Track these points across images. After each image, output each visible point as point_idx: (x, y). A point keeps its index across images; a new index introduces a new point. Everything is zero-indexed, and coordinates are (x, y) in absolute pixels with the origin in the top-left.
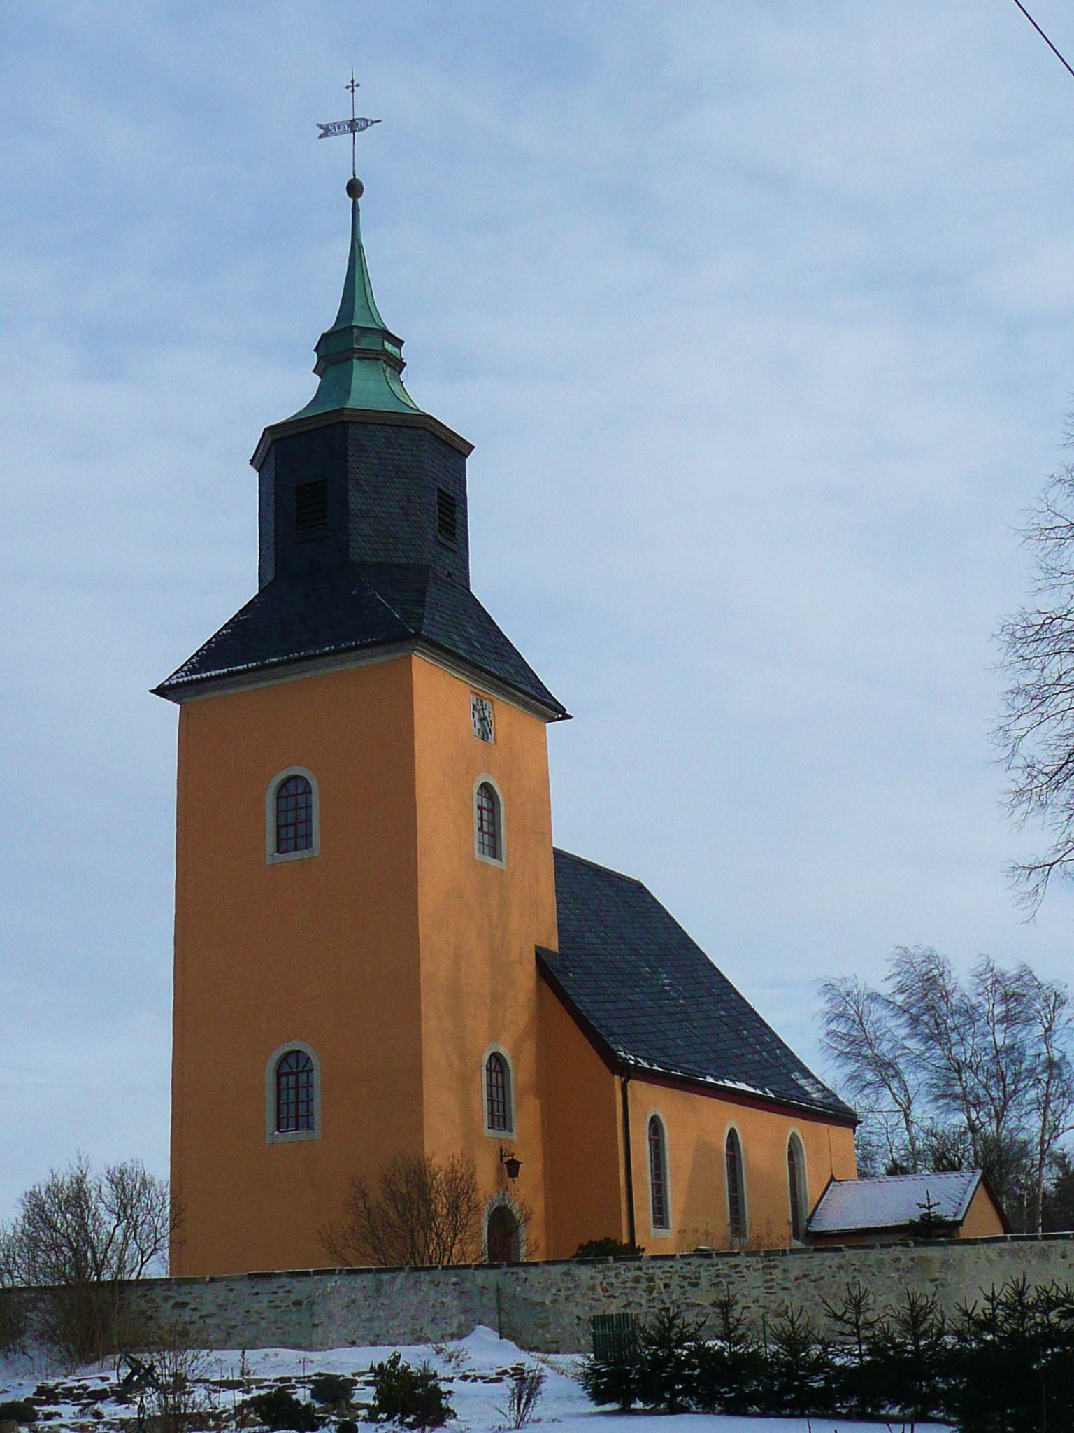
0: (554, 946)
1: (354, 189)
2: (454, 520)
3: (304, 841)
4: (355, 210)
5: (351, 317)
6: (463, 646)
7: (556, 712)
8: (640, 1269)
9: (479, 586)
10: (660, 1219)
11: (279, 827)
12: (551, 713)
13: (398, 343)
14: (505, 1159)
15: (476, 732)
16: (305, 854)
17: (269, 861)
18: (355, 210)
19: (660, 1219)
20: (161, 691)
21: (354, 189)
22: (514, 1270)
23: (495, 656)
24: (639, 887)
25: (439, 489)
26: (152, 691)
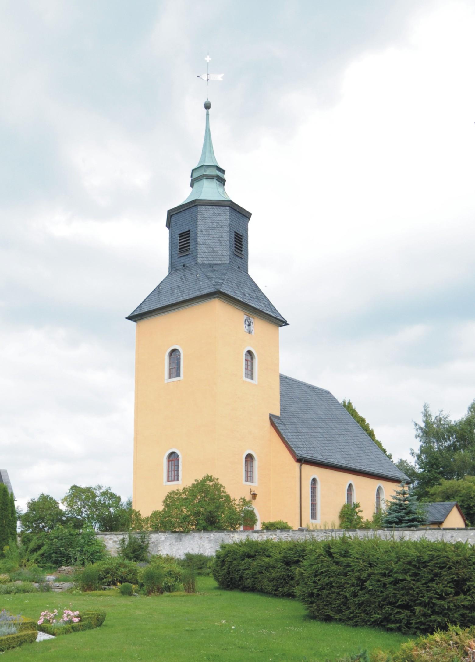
0: (278, 413)
1: (207, 106)
2: (242, 245)
3: (178, 375)
4: (208, 114)
5: (204, 161)
6: (241, 296)
7: (281, 322)
8: (276, 535)
9: (250, 273)
10: (314, 516)
11: (170, 369)
12: (280, 323)
13: (223, 172)
14: (252, 493)
15: (246, 330)
16: (178, 379)
17: (166, 382)
18: (208, 114)
19: (314, 516)
20: (130, 318)
21: (207, 106)
22: (229, 533)
23: (257, 300)
24: (328, 393)
25: (235, 232)
26: (127, 318)
